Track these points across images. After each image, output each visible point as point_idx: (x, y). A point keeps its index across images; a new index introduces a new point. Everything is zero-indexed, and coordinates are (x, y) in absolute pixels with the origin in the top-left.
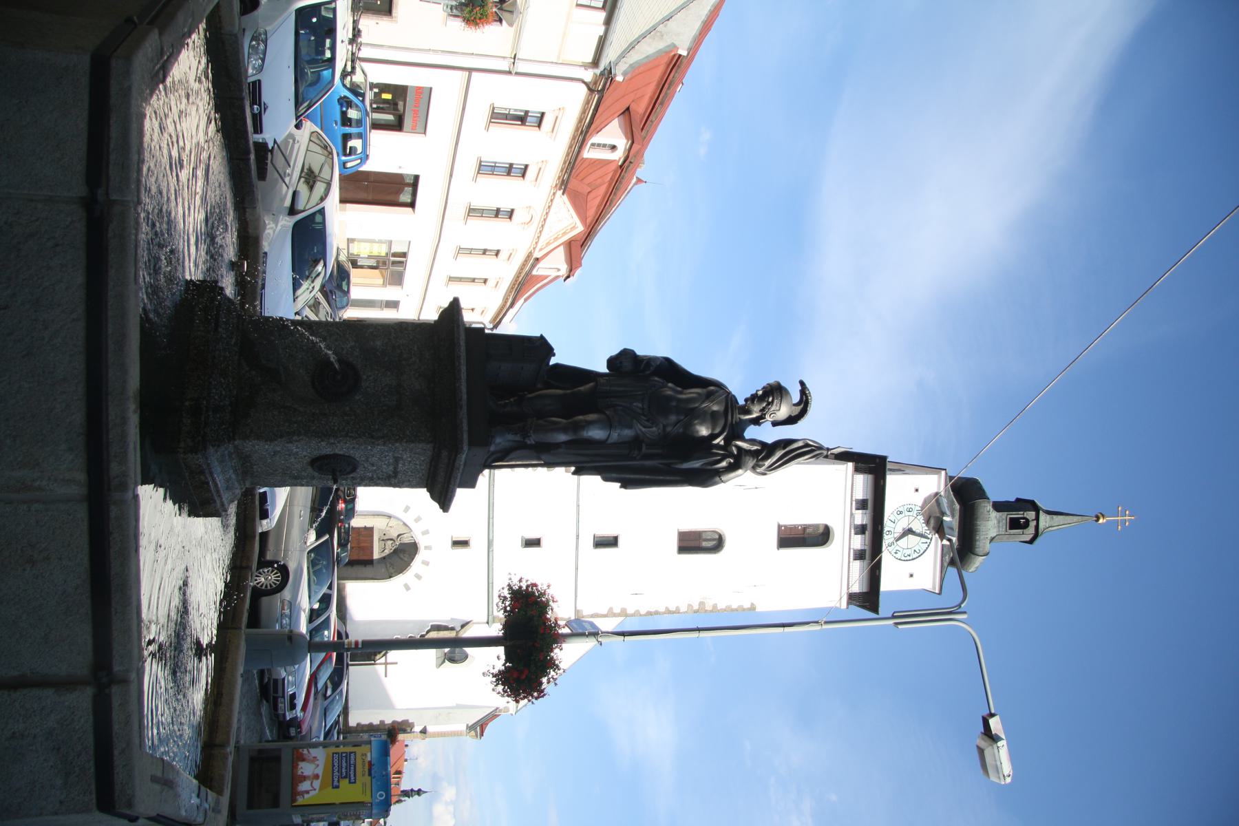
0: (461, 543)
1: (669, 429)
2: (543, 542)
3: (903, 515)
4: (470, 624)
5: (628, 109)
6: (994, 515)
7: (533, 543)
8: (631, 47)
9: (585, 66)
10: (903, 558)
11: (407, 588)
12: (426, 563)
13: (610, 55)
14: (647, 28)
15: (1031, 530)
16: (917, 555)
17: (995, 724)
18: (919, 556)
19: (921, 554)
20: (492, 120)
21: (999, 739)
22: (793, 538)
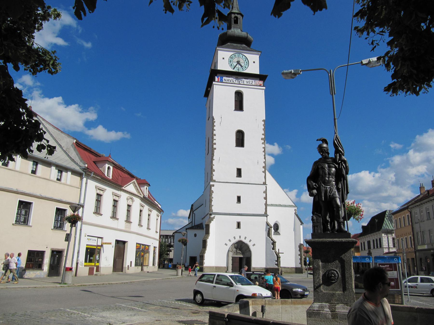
0: (239, 225)
1: (334, 180)
2: (239, 195)
3: (232, 64)
4: (268, 223)
5: (94, 162)
6: (232, 30)
7: (239, 199)
8: (73, 160)
9: (82, 179)
10: (248, 65)
11: (254, 245)
12: (245, 238)
13: (77, 168)
14: (65, 154)
15: (239, 16)
16: (247, 60)
17: (365, 62)
18: (247, 59)
19: (247, 58)
20: (98, 212)
21: (369, 61)
22: (239, 106)
